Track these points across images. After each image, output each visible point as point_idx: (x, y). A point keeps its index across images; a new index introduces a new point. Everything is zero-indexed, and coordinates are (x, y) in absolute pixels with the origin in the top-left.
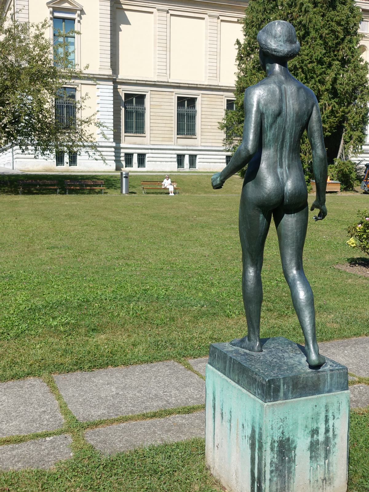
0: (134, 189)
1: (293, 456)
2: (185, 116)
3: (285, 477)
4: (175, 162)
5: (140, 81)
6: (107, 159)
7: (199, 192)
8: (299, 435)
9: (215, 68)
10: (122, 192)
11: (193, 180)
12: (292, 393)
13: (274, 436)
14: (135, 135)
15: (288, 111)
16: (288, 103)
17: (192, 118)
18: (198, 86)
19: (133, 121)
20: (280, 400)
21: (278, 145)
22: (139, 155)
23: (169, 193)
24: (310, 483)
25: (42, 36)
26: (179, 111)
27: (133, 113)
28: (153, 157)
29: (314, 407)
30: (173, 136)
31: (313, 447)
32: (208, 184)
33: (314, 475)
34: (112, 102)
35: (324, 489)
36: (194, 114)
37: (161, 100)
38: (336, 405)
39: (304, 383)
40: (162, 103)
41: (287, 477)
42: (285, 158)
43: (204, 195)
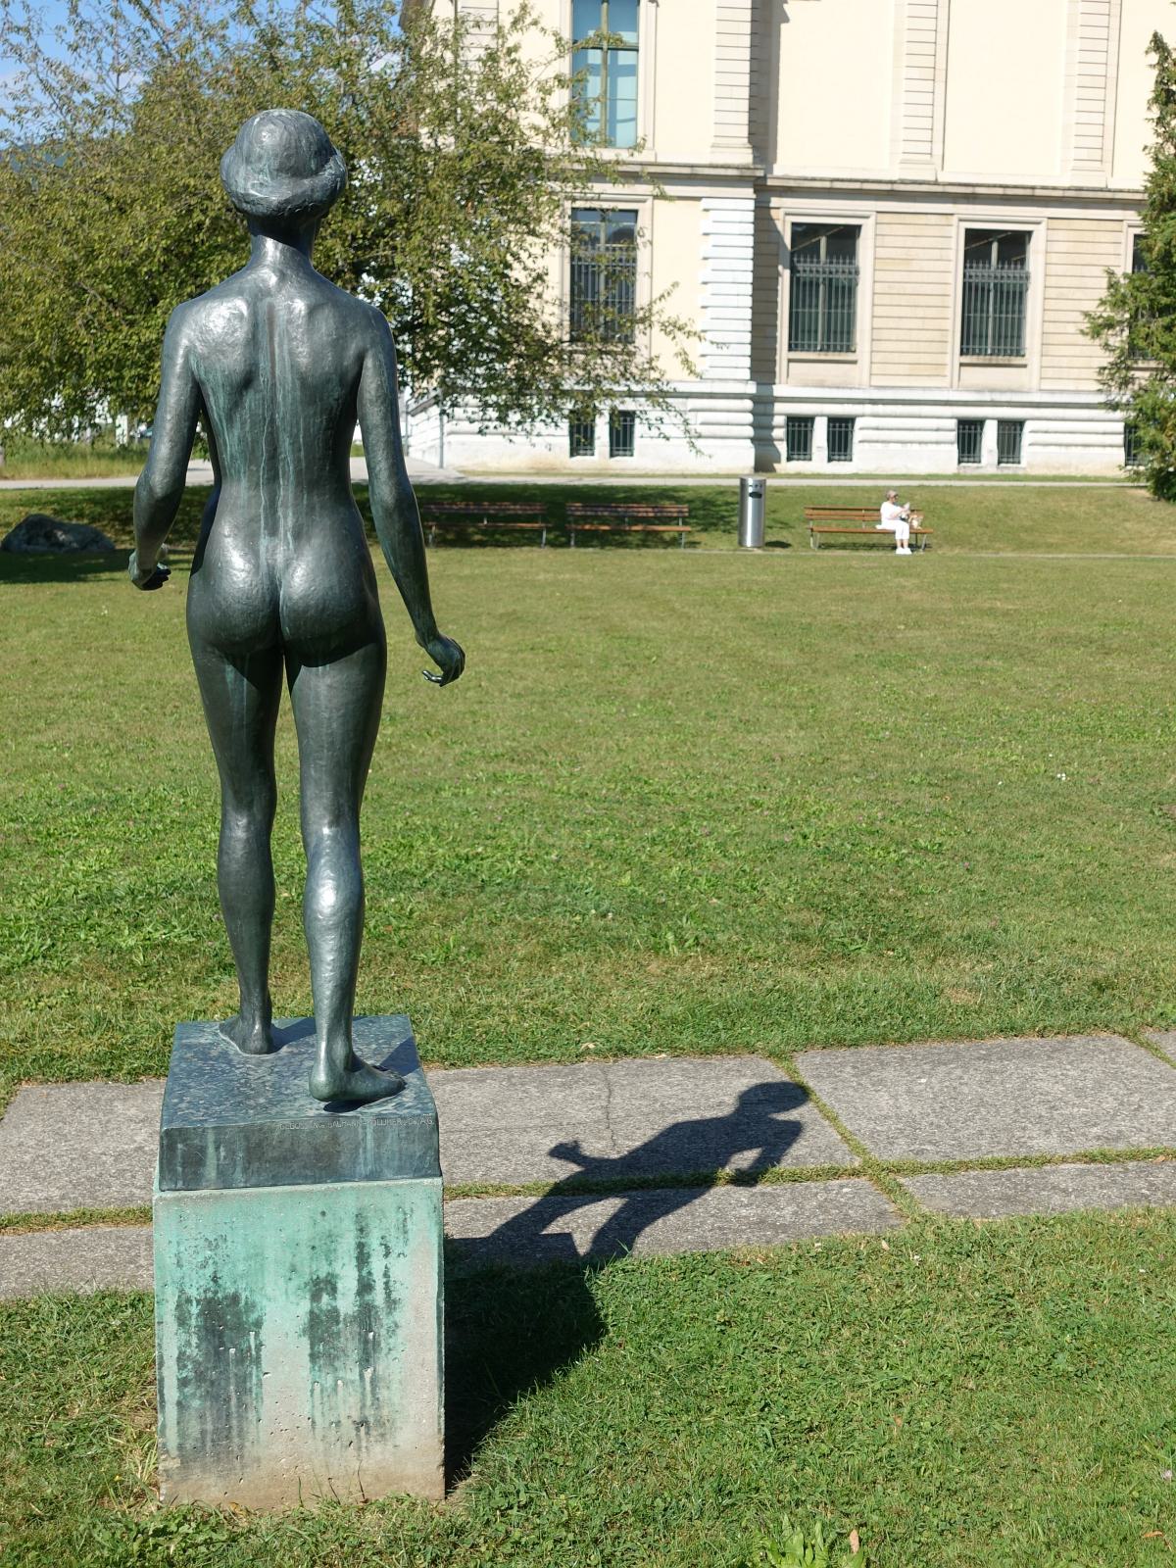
0: (785, 533)
1: (253, 1347)
2: (989, 291)
3: (227, 1401)
4: (952, 443)
5: (842, 180)
6: (703, 434)
7: (997, 545)
8: (269, 1290)
9: (1098, 130)
10: (741, 542)
11: (987, 504)
12: (245, 1170)
13: (188, 1285)
14: (822, 356)
15: (277, 372)
16: (277, 351)
17: (1013, 298)
18: (1038, 192)
19: (817, 313)
20: (207, 1188)
21: (258, 471)
22: (833, 421)
23: (894, 547)
24: (314, 1428)
25: (513, 55)
26: (970, 277)
27: (818, 285)
28: (877, 429)
29: (319, 1217)
30: (947, 359)
31: (320, 1329)
32: (1036, 517)
33: (326, 1408)
34: (750, 253)
35: (364, 1450)
36: (1021, 285)
37: (910, 242)
38: (393, 1218)
39: (287, 1145)
40: (913, 253)
41: (234, 1401)
42: (287, 507)
43: (1010, 555)
